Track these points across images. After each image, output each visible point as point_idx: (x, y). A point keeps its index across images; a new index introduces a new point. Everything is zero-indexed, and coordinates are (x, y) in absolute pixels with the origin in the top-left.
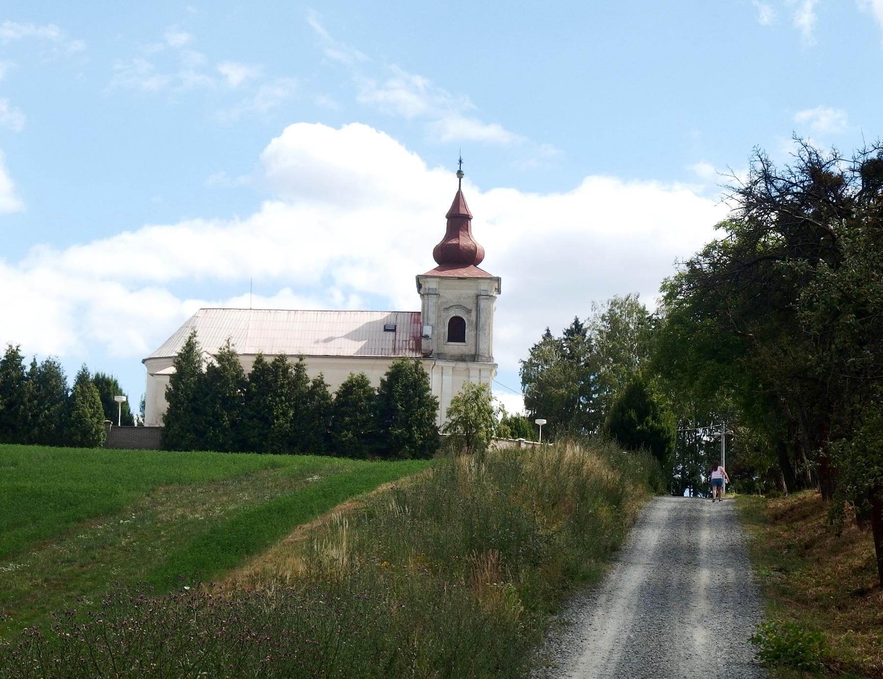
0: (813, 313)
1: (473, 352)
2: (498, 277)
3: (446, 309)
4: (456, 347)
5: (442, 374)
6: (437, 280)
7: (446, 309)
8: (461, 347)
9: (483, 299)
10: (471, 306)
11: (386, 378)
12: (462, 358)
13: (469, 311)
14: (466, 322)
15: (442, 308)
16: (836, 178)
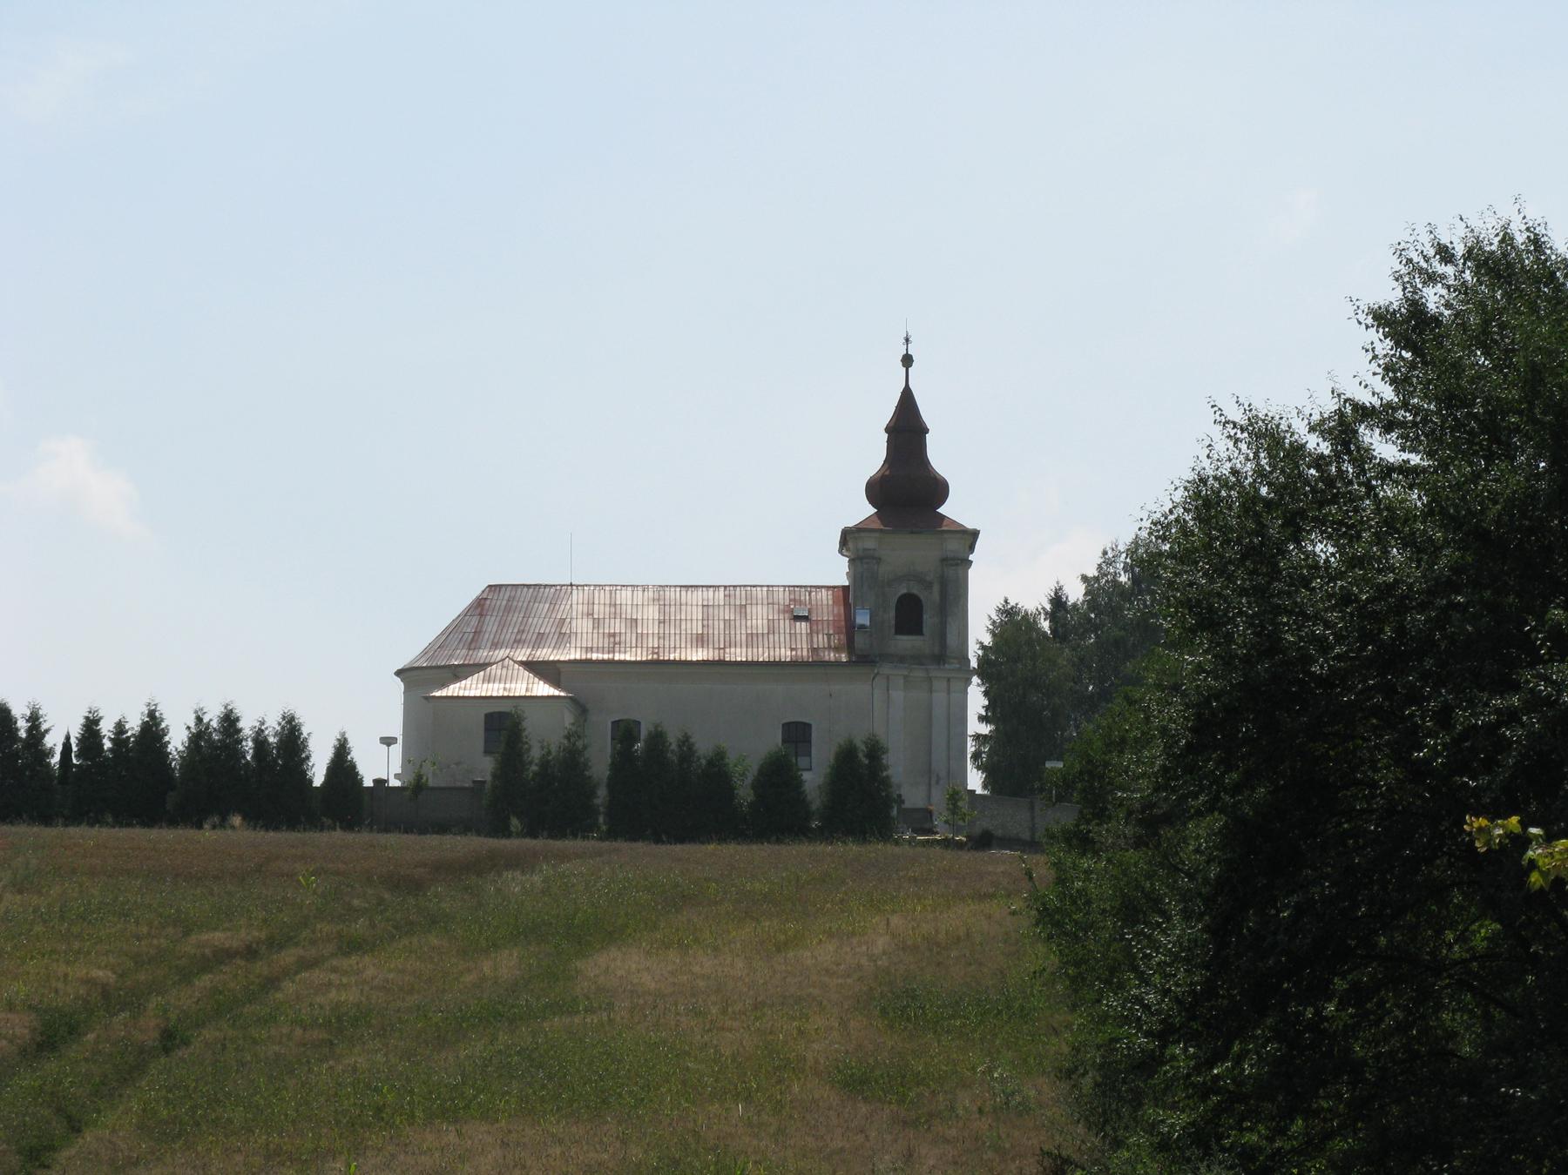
2: (975, 530)
6: (877, 535)
11: (1075, 593)
12: (918, 659)
13: (929, 586)
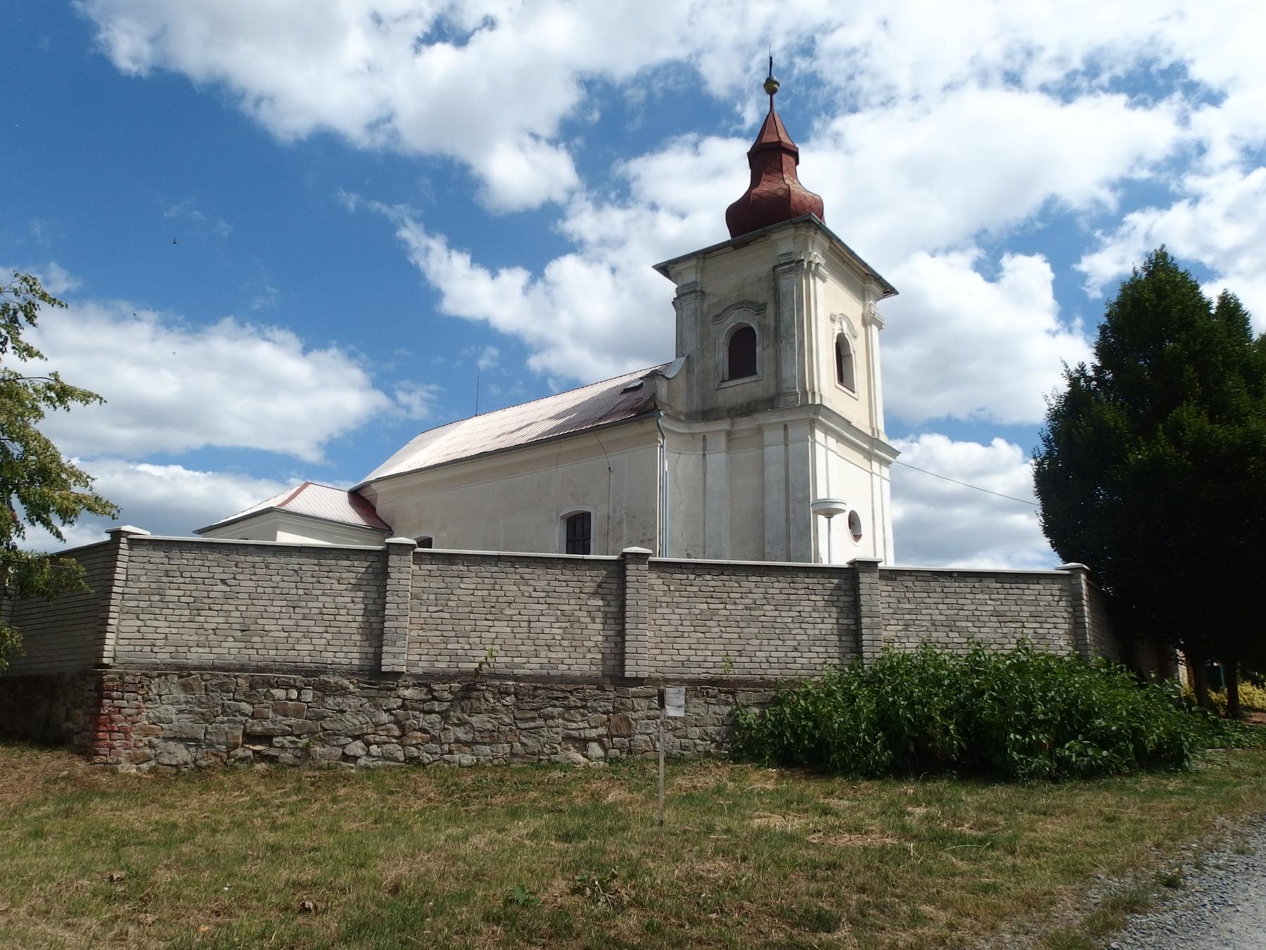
0: (873, 821)
1: (772, 391)
3: (717, 317)
4: (738, 389)
5: (704, 449)
7: (718, 316)
8: (748, 385)
9: (785, 272)
10: (764, 296)
13: (760, 309)
14: (756, 332)
15: (711, 317)
16: (275, 323)
